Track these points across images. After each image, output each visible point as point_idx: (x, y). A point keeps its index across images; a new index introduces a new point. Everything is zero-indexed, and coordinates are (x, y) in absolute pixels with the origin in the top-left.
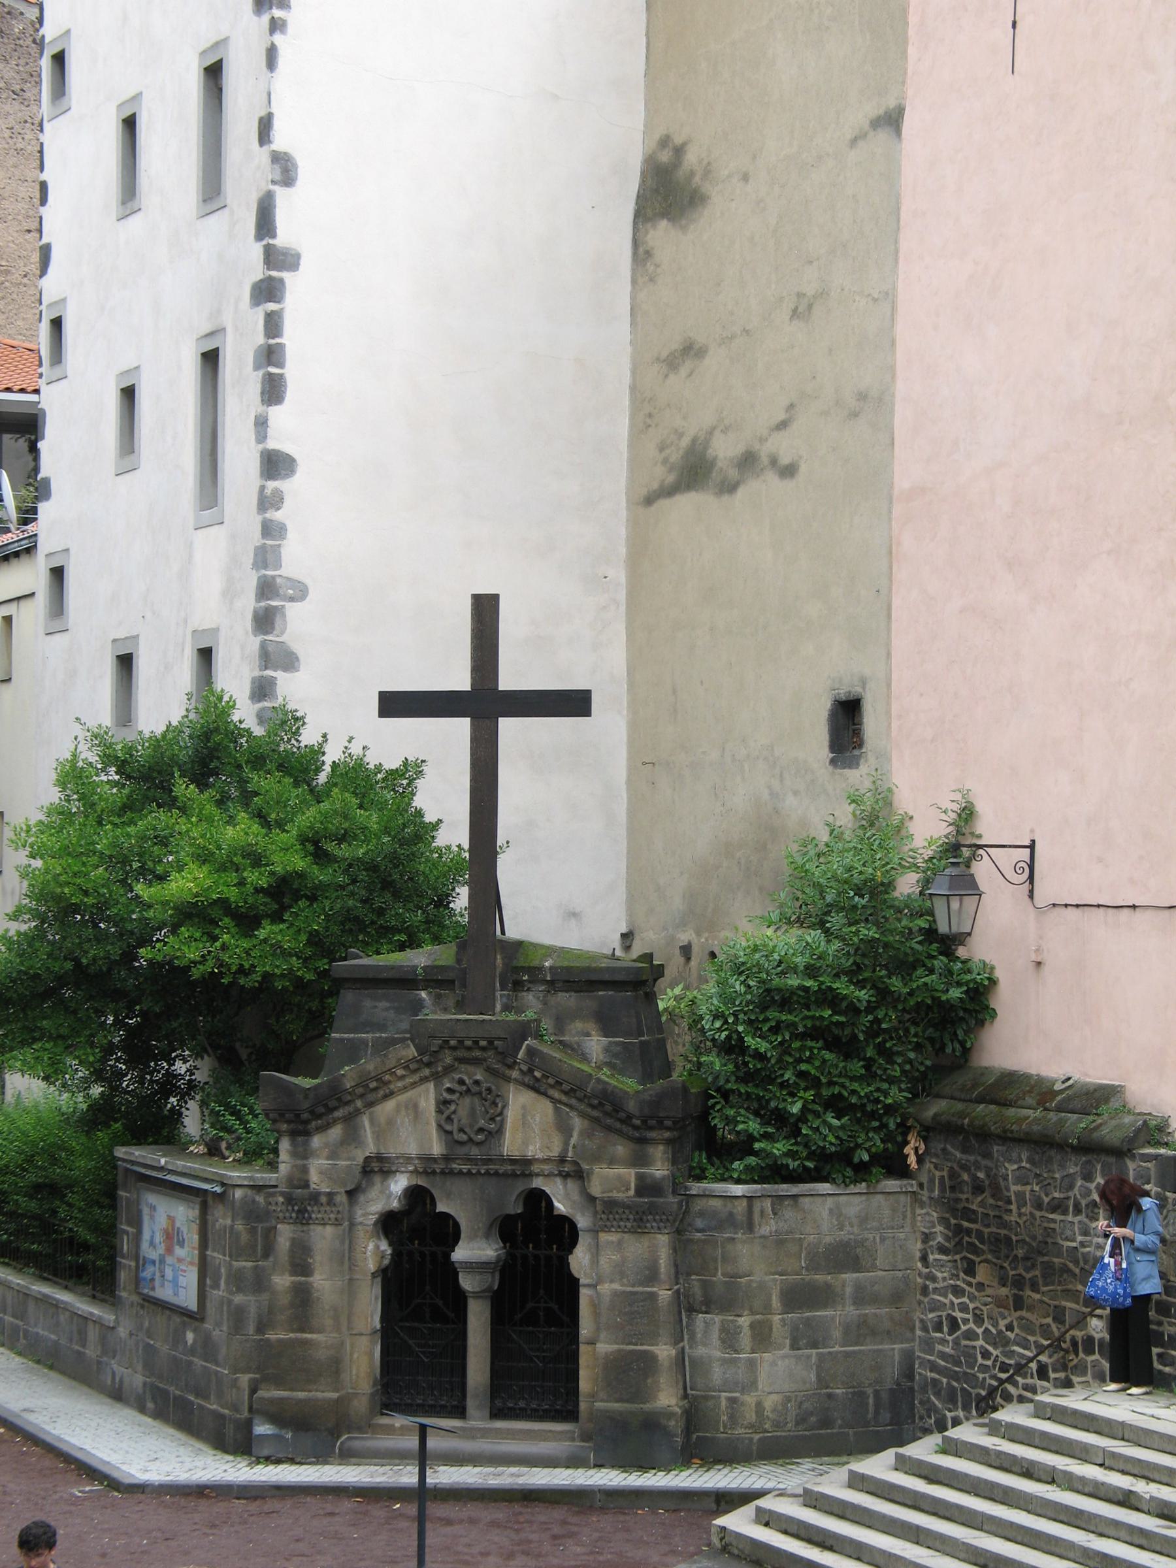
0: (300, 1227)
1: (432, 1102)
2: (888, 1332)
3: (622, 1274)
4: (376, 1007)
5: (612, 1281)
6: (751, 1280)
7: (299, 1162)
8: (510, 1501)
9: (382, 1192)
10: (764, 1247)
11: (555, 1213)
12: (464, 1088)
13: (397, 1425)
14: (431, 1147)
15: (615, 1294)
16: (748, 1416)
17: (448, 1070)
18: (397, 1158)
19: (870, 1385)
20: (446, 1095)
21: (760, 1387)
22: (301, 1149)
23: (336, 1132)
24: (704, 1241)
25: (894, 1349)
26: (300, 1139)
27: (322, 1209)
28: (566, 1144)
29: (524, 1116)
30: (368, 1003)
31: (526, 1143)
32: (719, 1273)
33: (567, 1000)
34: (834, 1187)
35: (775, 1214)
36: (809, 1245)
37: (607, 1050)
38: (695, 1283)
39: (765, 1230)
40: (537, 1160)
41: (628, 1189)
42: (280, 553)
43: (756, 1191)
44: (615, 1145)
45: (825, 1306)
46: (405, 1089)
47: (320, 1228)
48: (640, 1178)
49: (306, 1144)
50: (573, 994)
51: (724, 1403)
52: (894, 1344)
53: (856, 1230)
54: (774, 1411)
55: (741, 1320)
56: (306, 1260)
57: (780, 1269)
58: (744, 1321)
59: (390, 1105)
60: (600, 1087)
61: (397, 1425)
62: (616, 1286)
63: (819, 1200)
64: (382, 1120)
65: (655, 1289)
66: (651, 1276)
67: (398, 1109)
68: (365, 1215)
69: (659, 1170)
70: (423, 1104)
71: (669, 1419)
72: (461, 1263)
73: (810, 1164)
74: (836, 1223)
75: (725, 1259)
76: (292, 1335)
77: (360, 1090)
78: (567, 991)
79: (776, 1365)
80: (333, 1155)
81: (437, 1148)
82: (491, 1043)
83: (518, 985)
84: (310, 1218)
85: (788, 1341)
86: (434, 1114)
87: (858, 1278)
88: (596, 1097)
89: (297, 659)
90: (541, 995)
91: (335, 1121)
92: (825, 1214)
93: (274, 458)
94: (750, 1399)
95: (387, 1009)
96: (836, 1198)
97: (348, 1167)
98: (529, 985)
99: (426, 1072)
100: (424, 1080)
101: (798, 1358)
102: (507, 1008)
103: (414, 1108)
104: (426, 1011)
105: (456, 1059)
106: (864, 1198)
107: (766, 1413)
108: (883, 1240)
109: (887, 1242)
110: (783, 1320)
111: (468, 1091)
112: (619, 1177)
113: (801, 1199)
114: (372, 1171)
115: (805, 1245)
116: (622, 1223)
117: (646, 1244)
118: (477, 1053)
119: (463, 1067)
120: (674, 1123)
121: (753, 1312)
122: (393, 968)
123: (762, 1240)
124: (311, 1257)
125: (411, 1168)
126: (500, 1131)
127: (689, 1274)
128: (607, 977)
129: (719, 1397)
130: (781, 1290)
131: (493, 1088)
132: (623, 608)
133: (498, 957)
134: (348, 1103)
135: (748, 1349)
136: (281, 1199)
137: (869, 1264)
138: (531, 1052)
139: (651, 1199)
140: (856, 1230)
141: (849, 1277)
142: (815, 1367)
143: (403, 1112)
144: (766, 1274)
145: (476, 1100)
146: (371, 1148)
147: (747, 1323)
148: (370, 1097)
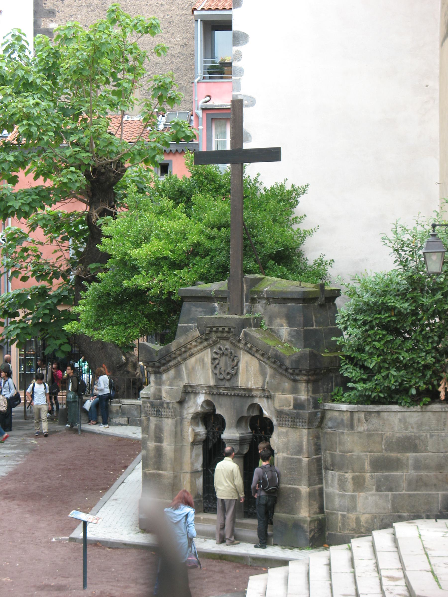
0: (159, 419)
1: (210, 359)
2: (435, 485)
3: (287, 449)
4: (196, 311)
5: (283, 452)
6: (353, 455)
7: (158, 387)
8: (214, 559)
9: (194, 403)
10: (360, 438)
11: (264, 416)
12: (222, 352)
13: (202, 518)
14: (209, 382)
15: (284, 458)
16: (351, 524)
17: (215, 343)
18: (198, 386)
19: (424, 512)
20: (215, 356)
21: (358, 510)
22: (158, 381)
23: (172, 372)
24: (332, 433)
25: (438, 494)
26: (158, 375)
27: (165, 410)
28: (264, 381)
29: (247, 367)
30: (194, 309)
31: (248, 381)
32: (338, 450)
33: (274, 307)
34: (401, 407)
35: (367, 420)
36: (387, 437)
37: (289, 334)
38: (328, 455)
39: (361, 429)
40: (253, 389)
41: (290, 405)
42: (240, 83)
43: (354, 408)
44: (284, 382)
45: (397, 470)
46: (198, 352)
47: (166, 420)
48: (295, 399)
49: (160, 378)
50: (277, 305)
51: (340, 517)
52: (438, 491)
53: (415, 430)
54: (366, 522)
55: (347, 475)
56: (160, 435)
57: (369, 449)
58: (349, 476)
59: (192, 360)
60: (275, 353)
61: (202, 518)
62: (285, 455)
63: (393, 414)
64: (190, 367)
65: (301, 457)
66: (299, 451)
67: (196, 362)
68: (188, 414)
69: (303, 396)
70: (206, 360)
71: (304, 524)
72: (225, 439)
73: (382, 395)
74: (403, 426)
75: (340, 443)
76: (155, 471)
77: (178, 352)
78: (275, 303)
79: (368, 499)
80: (171, 384)
81: (212, 383)
82: (230, 329)
83: (253, 300)
84: (162, 415)
85: (374, 487)
86: (210, 364)
87: (416, 456)
88: (273, 357)
89: (250, 136)
90: (264, 305)
91: (171, 367)
92: (397, 421)
93: (236, 35)
94: (352, 516)
95: (201, 312)
96: (403, 413)
97: (177, 390)
98: (259, 300)
99: (205, 344)
100: (205, 348)
101: (380, 496)
102: (249, 312)
103: (202, 361)
104: (216, 313)
105: (218, 337)
106: (420, 414)
107: (361, 523)
108: (431, 436)
109: (434, 437)
110: (372, 476)
111: (223, 354)
112: (286, 399)
113: (382, 414)
114: (189, 393)
115: (385, 437)
116: (287, 423)
117: (298, 434)
118: (225, 335)
119: (222, 341)
120: (306, 371)
121: (353, 471)
122: (202, 291)
123: (359, 434)
124: (163, 434)
125: (204, 392)
126: (236, 374)
127: (326, 450)
128: (290, 296)
129: (338, 514)
130: (370, 460)
131: (233, 352)
132: (437, 102)
133: (245, 286)
134: (175, 358)
135: (351, 490)
136: (149, 405)
137: (423, 449)
138: (246, 334)
139: (298, 411)
140: (415, 430)
141: (411, 455)
142: (391, 501)
143: (198, 364)
144: (361, 452)
145: (227, 358)
146: (185, 381)
147: (351, 477)
148: (184, 356)
